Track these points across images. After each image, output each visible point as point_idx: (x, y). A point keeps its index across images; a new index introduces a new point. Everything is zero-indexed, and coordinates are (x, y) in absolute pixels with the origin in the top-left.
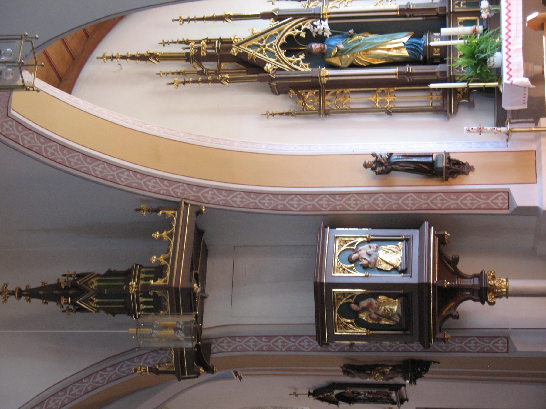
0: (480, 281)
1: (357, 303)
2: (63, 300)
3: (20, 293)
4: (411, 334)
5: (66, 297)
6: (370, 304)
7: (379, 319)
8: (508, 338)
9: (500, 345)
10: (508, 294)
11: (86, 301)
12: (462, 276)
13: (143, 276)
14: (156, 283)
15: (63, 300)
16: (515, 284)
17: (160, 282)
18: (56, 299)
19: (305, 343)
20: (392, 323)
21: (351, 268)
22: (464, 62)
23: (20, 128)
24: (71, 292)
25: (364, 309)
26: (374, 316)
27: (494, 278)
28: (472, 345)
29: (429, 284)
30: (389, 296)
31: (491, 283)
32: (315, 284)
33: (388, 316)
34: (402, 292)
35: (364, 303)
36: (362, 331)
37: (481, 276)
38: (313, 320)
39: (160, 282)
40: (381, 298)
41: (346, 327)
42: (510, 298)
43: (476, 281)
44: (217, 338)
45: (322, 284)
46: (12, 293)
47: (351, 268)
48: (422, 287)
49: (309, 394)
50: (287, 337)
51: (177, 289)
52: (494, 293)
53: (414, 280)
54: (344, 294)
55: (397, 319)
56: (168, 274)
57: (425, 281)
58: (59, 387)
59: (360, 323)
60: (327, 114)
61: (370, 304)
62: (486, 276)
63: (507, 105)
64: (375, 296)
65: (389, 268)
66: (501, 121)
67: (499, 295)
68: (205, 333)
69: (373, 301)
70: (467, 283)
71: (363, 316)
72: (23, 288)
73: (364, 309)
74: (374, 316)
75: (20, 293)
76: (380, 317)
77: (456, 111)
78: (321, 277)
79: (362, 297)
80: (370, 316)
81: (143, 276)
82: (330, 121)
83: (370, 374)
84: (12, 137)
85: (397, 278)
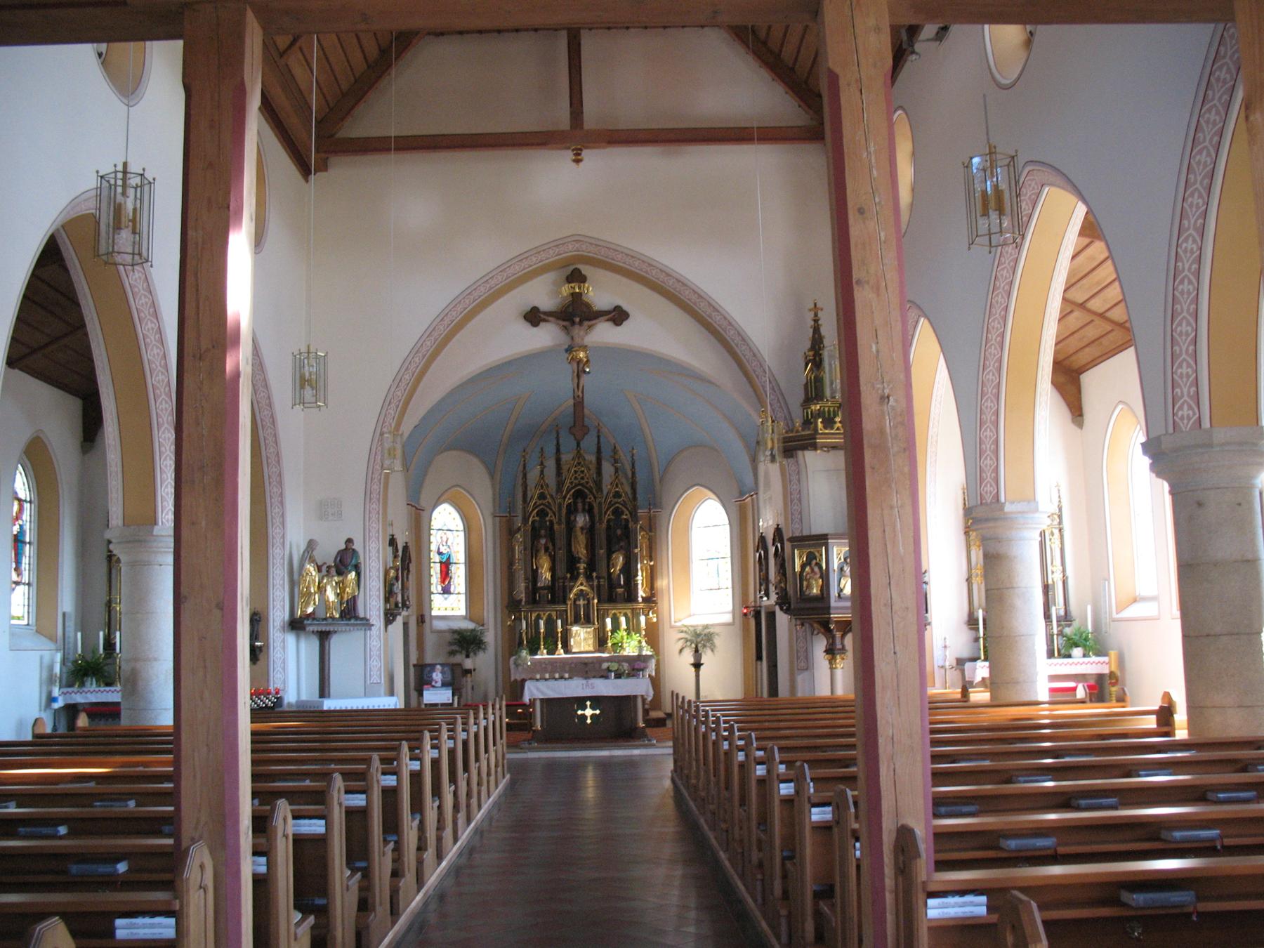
0: (840, 649)
1: (817, 564)
2: (811, 353)
3: (816, 321)
4: (797, 603)
5: (814, 355)
6: (815, 574)
7: (806, 580)
8: (807, 669)
9: (802, 664)
10: (831, 668)
11: (811, 369)
12: (843, 637)
13: (832, 409)
14: (819, 424)
15: (811, 353)
16: (839, 673)
17: (820, 425)
18: (812, 348)
19: (797, 526)
20: (804, 589)
21: (840, 559)
22: (455, 639)
23: (1012, 264)
24: (817, 359)
25: (812, 570)
26: (808, 577)
27: (843, 659)
28: (801, 644)
29: (830, 614)
30: (822, 587)
31: (838, 657)
32: (826, 535)
33: (809, 586)
34: (825, 595)
35: (816, 569)
36: (798, 568)
37: (843, 650)
38: (814, 532)
39: (820, 425)
40: (820, 581)
41: (800, 557)
42: (829, 671)
43: (839, 646)
44: (797, 462)
45: (827, 539)
46: (816, 315)
47: (840, 559)
48: (827, 609)
49: (778, 525)
50: (800, 513)
51: (815, 439)
52: (832, 659)
53: (833, 603)
54: (821, 555)
55: (807, 593)
56: (827, 431)
57: (832, 611)
58: (755, 351)
59: (803, 566)
60: (966, 533)
61: (815, 574)
62: (844, 653)
63: (968, 665)
64: (821, 577)
65: (842, 586)
66: (960, 662)
67: (830, 663)
68: (800, 453)
69: (818, 576)
70: (838, 641)
71: (808, 569)
72: (820, 322)
73: (812, 570)
74: (808, 577)
75: (816, 321)
76: (808, 580)
77: (971, 629)
78: (832, 539)
79: (820, 568)
80: (808, 574)
81: (832, 409)
82: (962, 537)
83: (779, 573)
84: (1003, 260)
85: (834, 592)
